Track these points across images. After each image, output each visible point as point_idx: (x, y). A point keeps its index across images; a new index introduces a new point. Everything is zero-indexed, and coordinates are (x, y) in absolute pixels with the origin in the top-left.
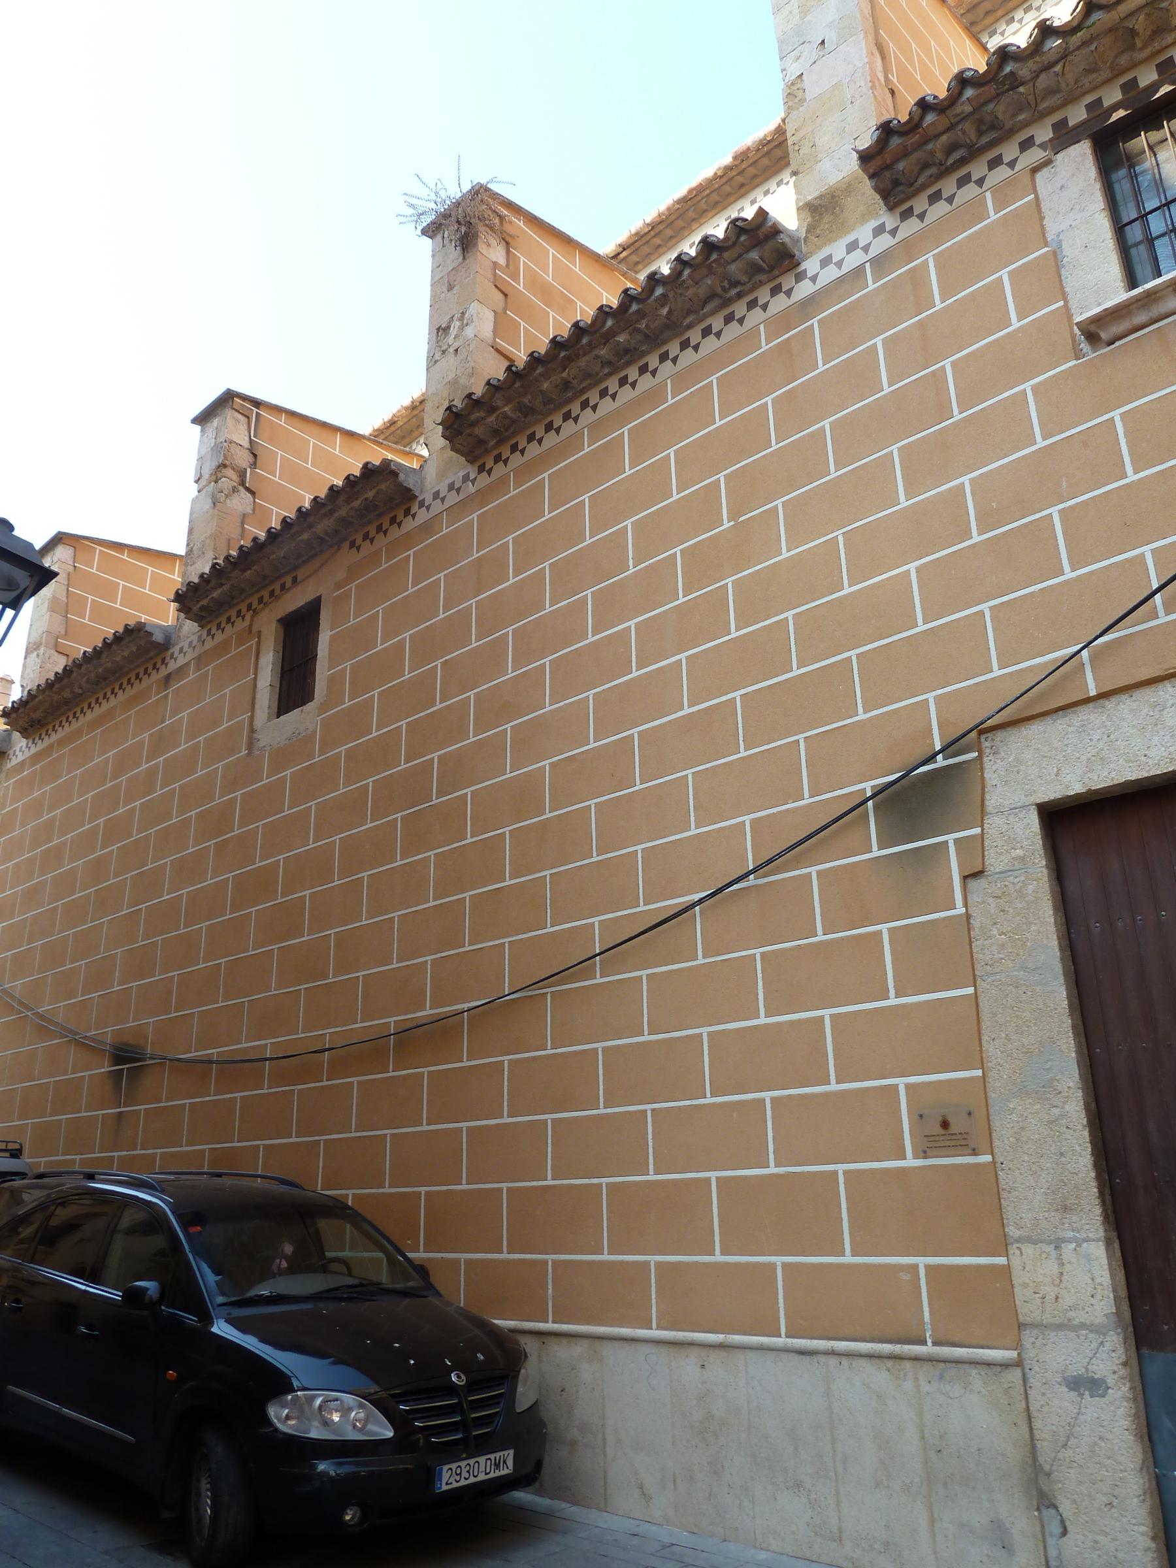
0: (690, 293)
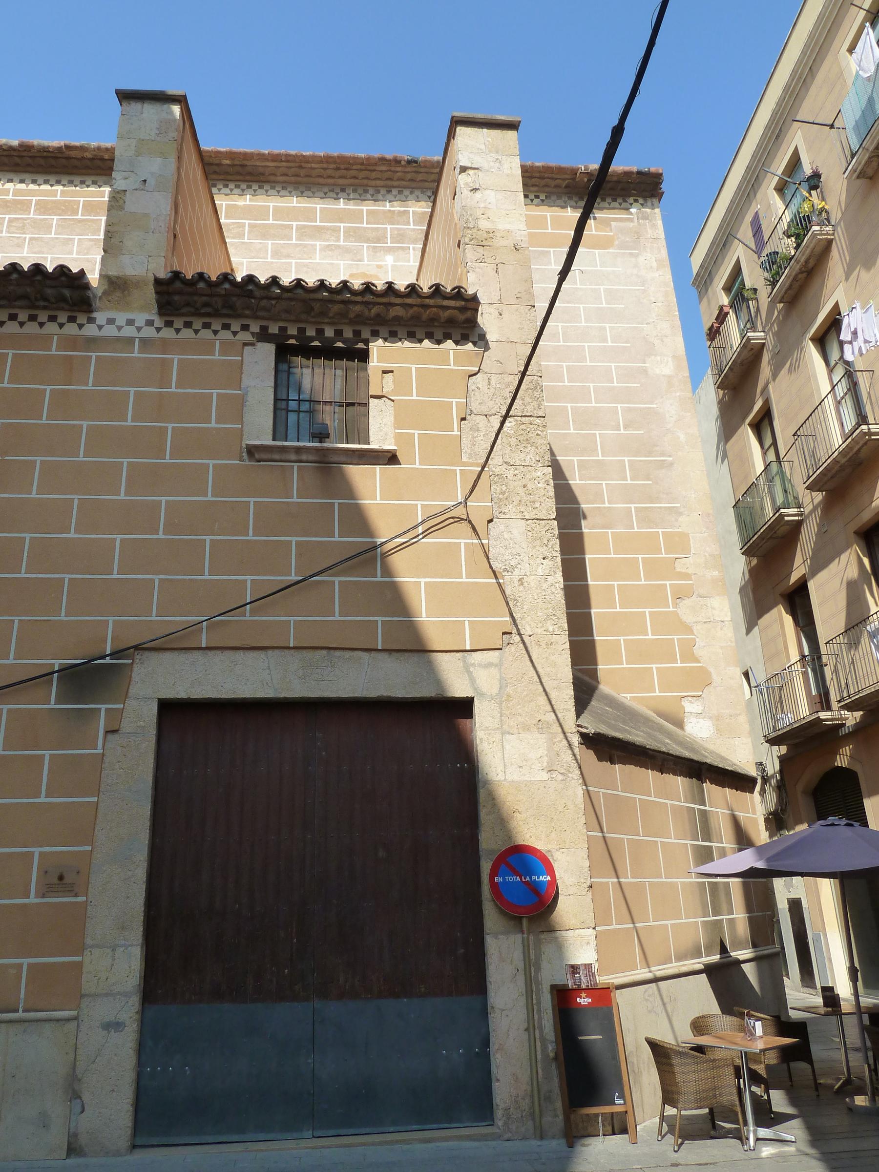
0: (11, 288)
